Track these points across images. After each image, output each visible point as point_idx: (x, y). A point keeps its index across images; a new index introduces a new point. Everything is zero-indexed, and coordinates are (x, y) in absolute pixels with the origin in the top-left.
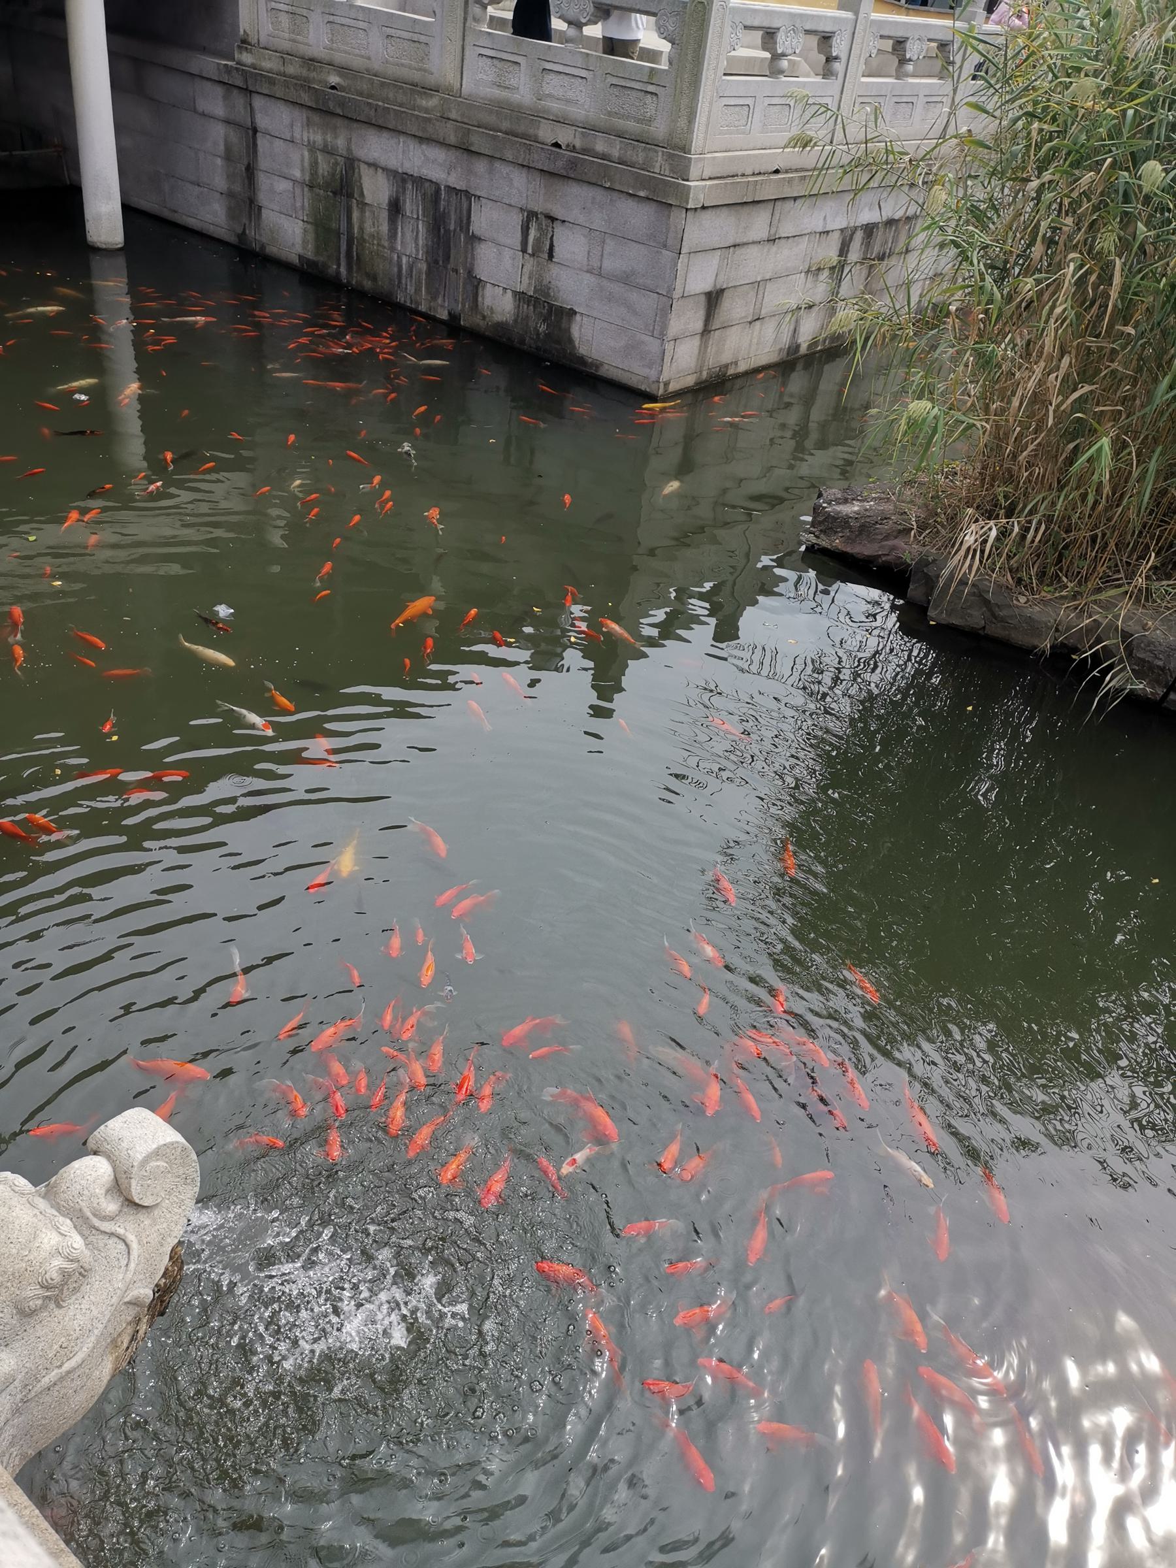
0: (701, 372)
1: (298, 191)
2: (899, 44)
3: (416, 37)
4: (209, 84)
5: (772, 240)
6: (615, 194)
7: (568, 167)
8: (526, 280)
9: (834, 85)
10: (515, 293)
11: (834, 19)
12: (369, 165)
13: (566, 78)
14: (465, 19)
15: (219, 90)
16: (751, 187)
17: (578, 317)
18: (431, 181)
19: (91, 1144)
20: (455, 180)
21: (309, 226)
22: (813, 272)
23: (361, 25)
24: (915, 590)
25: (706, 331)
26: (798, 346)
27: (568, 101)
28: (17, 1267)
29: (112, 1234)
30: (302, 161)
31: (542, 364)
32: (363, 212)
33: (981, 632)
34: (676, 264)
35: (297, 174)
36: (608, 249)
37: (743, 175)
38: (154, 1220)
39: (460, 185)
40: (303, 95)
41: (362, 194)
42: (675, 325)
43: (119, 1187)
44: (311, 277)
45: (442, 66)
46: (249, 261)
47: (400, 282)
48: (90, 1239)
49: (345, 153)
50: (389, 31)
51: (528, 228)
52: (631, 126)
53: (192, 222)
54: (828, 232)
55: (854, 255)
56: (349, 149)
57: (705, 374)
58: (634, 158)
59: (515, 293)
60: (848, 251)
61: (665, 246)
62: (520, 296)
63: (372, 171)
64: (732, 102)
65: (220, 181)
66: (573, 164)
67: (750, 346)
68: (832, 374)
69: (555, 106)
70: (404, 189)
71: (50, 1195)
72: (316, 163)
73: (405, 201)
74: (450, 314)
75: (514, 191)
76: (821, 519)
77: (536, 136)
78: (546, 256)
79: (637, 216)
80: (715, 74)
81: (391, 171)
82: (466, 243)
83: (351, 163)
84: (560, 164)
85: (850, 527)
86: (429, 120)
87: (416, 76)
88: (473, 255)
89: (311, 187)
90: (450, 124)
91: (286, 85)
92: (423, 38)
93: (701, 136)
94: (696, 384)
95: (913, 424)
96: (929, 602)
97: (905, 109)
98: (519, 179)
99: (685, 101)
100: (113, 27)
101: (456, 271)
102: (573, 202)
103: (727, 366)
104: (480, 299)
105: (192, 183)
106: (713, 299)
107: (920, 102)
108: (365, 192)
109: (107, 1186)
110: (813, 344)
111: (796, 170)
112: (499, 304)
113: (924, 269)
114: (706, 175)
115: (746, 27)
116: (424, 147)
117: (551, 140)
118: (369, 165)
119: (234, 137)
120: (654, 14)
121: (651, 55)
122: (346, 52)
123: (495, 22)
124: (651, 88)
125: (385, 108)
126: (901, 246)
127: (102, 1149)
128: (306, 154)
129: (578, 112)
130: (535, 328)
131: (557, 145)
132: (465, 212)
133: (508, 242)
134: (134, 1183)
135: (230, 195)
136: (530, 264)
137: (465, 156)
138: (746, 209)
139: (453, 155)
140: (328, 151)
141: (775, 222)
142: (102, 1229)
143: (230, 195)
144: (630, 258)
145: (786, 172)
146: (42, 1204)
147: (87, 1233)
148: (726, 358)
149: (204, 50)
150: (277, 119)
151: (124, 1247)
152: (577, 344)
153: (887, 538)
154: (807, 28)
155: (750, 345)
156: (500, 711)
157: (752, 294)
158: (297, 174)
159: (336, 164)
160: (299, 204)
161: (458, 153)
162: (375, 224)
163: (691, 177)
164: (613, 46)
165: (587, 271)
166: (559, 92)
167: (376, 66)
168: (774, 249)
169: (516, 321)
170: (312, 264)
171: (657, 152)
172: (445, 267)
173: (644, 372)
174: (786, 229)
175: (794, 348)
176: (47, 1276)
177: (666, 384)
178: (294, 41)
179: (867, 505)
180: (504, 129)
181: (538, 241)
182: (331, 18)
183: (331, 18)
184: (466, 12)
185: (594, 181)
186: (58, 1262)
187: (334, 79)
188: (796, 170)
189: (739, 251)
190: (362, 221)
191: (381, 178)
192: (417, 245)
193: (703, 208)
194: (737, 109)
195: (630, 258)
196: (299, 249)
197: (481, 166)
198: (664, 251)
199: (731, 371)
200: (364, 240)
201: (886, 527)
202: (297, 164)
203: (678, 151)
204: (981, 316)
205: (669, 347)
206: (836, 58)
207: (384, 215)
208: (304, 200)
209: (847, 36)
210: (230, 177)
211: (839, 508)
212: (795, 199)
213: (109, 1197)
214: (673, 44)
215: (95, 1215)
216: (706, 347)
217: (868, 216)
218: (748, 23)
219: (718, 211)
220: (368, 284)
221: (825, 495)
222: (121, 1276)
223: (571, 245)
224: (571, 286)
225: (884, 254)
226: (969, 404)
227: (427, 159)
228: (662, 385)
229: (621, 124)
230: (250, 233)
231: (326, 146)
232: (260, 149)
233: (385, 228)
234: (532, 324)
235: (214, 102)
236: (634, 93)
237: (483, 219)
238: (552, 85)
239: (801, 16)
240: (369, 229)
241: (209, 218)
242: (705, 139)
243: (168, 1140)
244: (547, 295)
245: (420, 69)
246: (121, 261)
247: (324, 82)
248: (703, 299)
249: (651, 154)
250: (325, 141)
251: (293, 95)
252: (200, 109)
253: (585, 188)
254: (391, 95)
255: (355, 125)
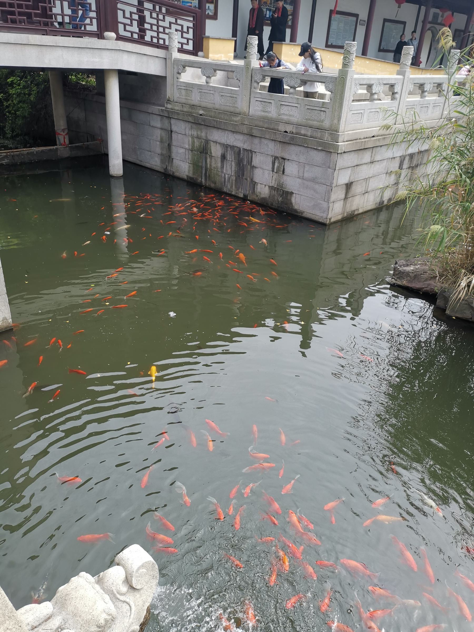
0: (344, 214)
1: (187, 152)
2: (421, 86)
3: (232, 96)
4: (155, 116)
5: (372, 162)
6: (309, 149)
7: (291, 139)
8: (274, 182)
9: (396, 103)
10: (269, 187)
11: (395, 79)
12: (214, 142)
13: (290, 107)
14: (251, 88)
15: (159, 118)
16: (363, 143)
17: (294, 195)
18: (237, 147)
19: (117, 560)
20: (246, 146)
21: (191, 165)
22: (389, 173)
23: (212, 92)
24: (440, 302)
25: (346, 198)
26: (383, 202)
27: (290, 115)
28: (88, 617)
29: (124, 601)
30: (189, 141)
31: (282, 213)
32: (211, 159)
33: (470, 320)
34: (334, 174)
35: (187, 146)
36: (306, 169)
37: (360, 139)
38: (141, 595)
39: (249, 148)
40: (189, 118)
41: (211, 153)
42: (333, 197)
43: (128, 581)
44: (192, 184)
45: (242, 106)
46: (168, 178)
47: (225, 184)
48: (116, 603)
49: (205, 138)
50: (222, 94)
51: (274, 163)
52: (315, 123)
53: (148, 165)
54: (394, 158)
55: (405, 165)
56: (206, 137)
57: (345, 214)
58: (317, 136)
59: (269, 187)
60: (403, 164)
61: (329, 167)
62: (271, 188)
63: (215, 144)
64: (355, 112)
65: (158, 150)
66: (292, 138)
67: (364, 203)
68: (397, 212)
69: (285, 117)
70: (227, 151)
71: (100, 582)
72: (194, 142)
73: (227, 155)
74: (244, 195)
75: (269, 149)
76: (397, 273)
77: (278, 129)
78: (282, 173)
79: (318, 157)
80: (349, 103)
81: (222, 144)
82: (250, 169)
83: (207, 141)
84: (287, 139)
85: (410, 276)
86: (237, 125)
87: (232, 109)
88: (253, 173)
89: (192, 151)
90: (244, 126)
91: (184, 115)
92: (234, 96)
93: (343, 126)
94: (342, 218)
95: (434, 235)
96: (446, 307)
97: (425, 109)
98: (271, 145)
99: (336, 114)
100: (122, 98)
101: (247, 179)
102: (293, 153)
103: (354, 211)
104: (256, 189)
105: (148, 151)
106: (348, 186)
107: (431, 106)
108: (212, 152)
109: (123, 580)
110: (390, 200)
111: (381, 136)
112: (263, 191)
113: (433, 171)
114: (345, 140)
115: (360, 85)
116: (235, 134)
117: (284, 130)
118: (214, 142)
119: (164, 134)
120: (324, 83)
121: (322, 96)
122: (206, 102)
123: (263, 88)
124: (323, 109)
125: (220, 121)
126: (425, 161)
127: (121, 563)
128: (190, 139)
129: (294, 120)
130: (277, 200)
131: (286, 132)
132: (250, 158)
133: (267, 168)
134: (133, 579)
135: (162, 155)
136: (275, 176)
137: (250, 137)
138: (362, 151)
139: (246, 137)
140: (198, 137)
141: (373, 155)
142: (121, 599)
143: (162, 155)
144: (316, 172)
145: (377, 136)
146: (97, 587)
147: (114, 601)
148: (354, 208)
149: (154, 104)
150: (179, 127)
151: (129, 607)
152: (294, 204)
153: (426, 280)
154: (385, 83)
155: (363, 202)
156: (262, 348)
157: (364, 183)
158: (187, 146)
159: (201, 142)
160: (187, 157)
161: (248, 136)
162: (215, 163)
163: (339, 141)
164: (307, 95)
165: (298, 178)
166: (287, 113)
167: (217, 106)
168: (373, 165)
169: (269, 197)
170: (190, 178)
171: (326, 133)
172: (242, 178)
173: (322, 215)
174: (378, 158)
175: (382, 202)
176: (100, 622)
177: (330, 219)
178: (186, 99)
179: (417, 267)
180: (265, 127)
181: (278, 167)
182: (201, 91)
183: (201, 91)
184: (251, 86)
185: (300, 144)
186: (104, 616)
187: (201, 112)
188: (381, 136)
189: (359, 167)
190: (211, 162)
191: (218, 147)
192: (231, 170)
193: (344, 152)
194: (357, 114)
195: (316, 172)
196: (187, 173)
197: (256, 141)
198: (329, 169)
199: (356, 213)
200: (212, 169)
201: (425, 276)
202: (187, 143)
203: (334, 132)
204: (463, 192)
205: (331, 205)
206: (396, 93)
207: (219, 160)
208: (189, 156)
209: (400, 84)
210: (162, 149)
211: (405, 268)
212: (381, 146)
213: (123, 585)
214: (332, 93)
215: (118, 593)
216: (346, 204)
217: (411, 151)
218: (361, 83)
219: (350, 153)
220: (213, 185)
221: (398, 263)
222: (127, 620)
223: (291, 168)
224: (291, 183)
225: (418, 164)
226: (459, 227)
227: (236, 139)
228: (328, 220)
229: (311, 123)
230: (169, 168)
231: (198, 136)
232: (173, 138)
233: (219, 165)
234: (276, 198)
235: (157, 122)
236: (317, 112)
237: (257, 160)
238: (284, 110)
239: (382, 79)
240: (213, 165)
241: (154, 163)
242: (345, 127)
243: (149, 560)
244: (282, 187)
245: (233, 107)
246: (122, 180)
247: (198, 113)
248: (344, 186)
249: (323, 133)
250: (197, 134)
251: (186, 118)
252: (152, 125)
253: (297, 147)
254: (222, 117)
255: (209, 128)
